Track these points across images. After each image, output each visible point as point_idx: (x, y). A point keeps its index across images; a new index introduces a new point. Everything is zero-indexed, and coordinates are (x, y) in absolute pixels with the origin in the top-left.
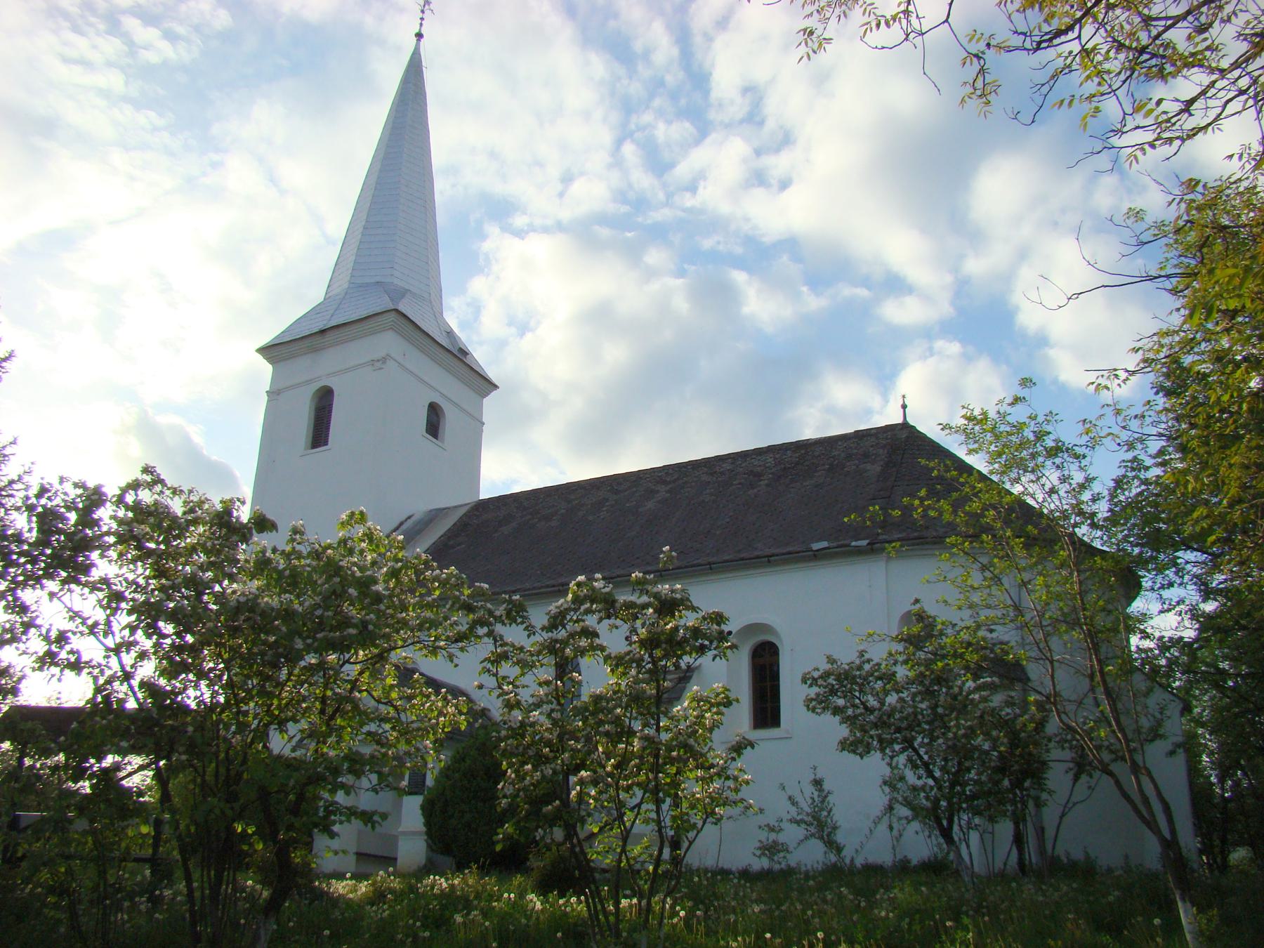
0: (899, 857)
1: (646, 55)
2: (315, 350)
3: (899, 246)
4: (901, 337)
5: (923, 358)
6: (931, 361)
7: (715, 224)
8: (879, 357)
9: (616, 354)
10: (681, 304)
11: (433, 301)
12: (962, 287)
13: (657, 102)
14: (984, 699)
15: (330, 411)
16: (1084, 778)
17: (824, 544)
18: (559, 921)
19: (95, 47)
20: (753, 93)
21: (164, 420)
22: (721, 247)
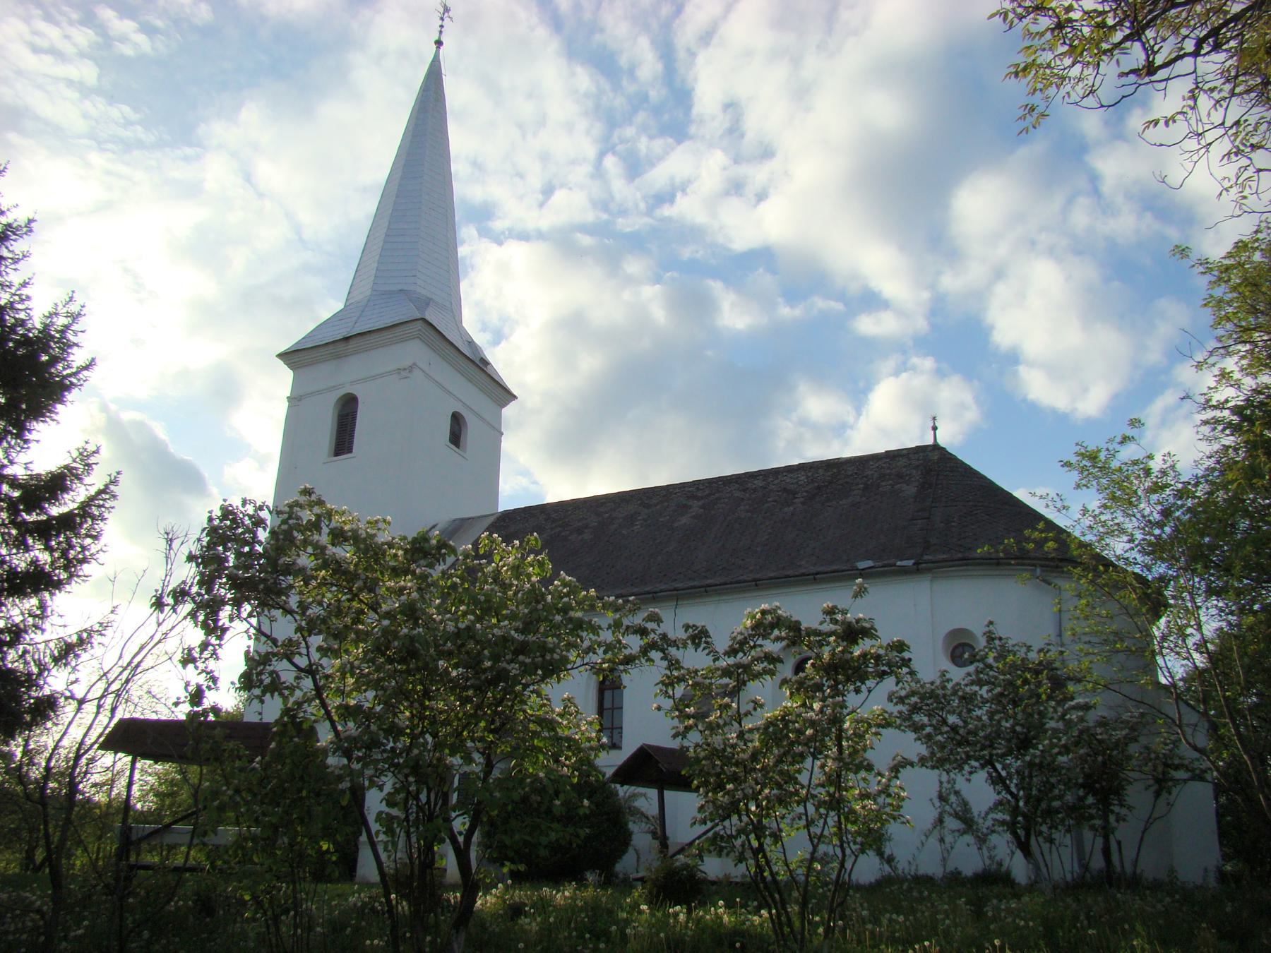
0: (950, 867)
1: (631, 72)
2: (338, 357)
3: (878, 263)
4: (873, 348)
5: (896, 373)
6: (904, 375)
7: (693, 233)
8: (851, 372)
9: (590, 363)
10: (659, 314)
11: (453, 306)
12: (938, 307)
13: (641, 117)
14: (1081, 719)
15: (354, 418)
16: (1164, 794)
17: (870, 563)
18: (737, 933)
19: (67, 37)
20: (732, 107)
21: (128, 416)
22: (698, 256)
